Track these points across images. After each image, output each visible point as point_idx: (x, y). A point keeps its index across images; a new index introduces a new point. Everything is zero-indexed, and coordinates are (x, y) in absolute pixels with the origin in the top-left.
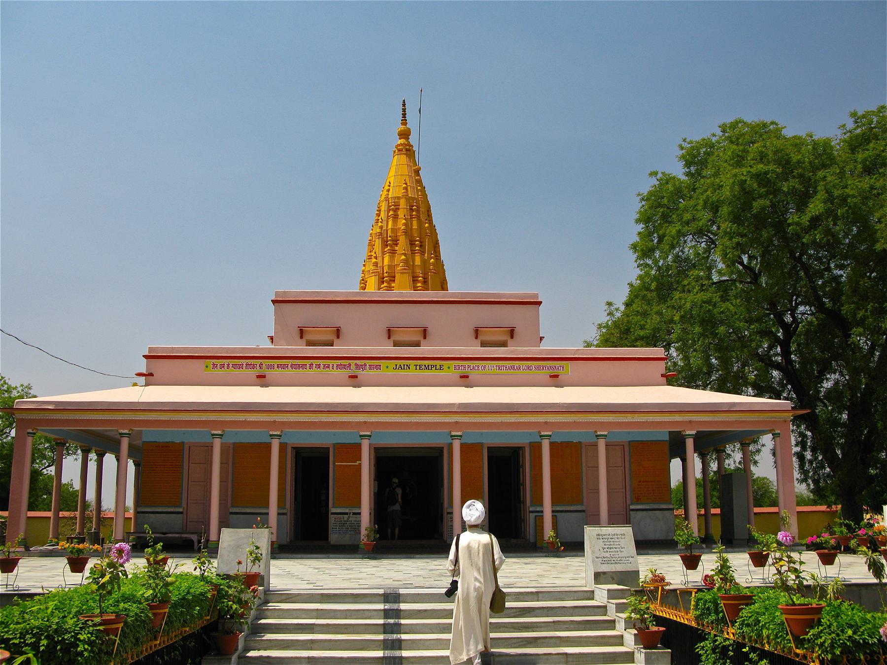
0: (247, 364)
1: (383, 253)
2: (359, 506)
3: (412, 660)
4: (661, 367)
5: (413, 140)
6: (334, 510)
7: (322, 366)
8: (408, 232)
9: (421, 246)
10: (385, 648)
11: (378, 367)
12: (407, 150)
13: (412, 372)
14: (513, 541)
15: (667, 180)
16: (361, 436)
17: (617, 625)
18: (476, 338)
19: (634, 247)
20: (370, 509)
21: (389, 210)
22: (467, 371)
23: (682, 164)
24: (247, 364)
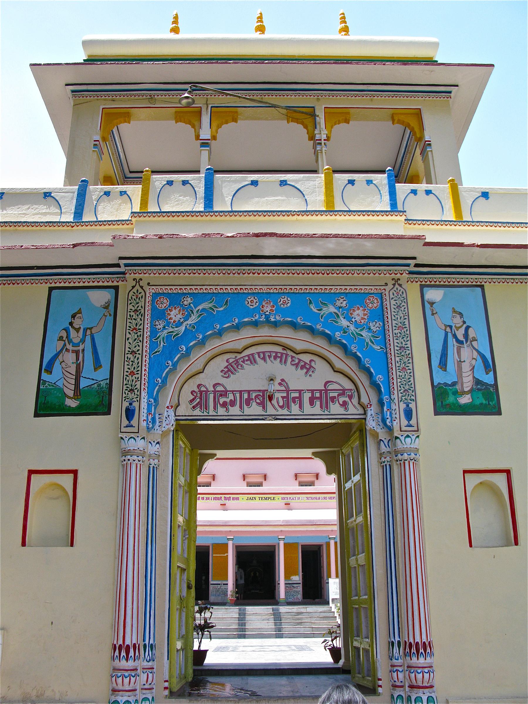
0: (225, 497)
2: (227, 579)
6: (212, 582)
7: (205, 499)
11: (238, 499)
13: (257, 502)
16: (228, 539)
18: (244, 480)
20: (233, 581)
22: (289, 501)
24: (225, 497)
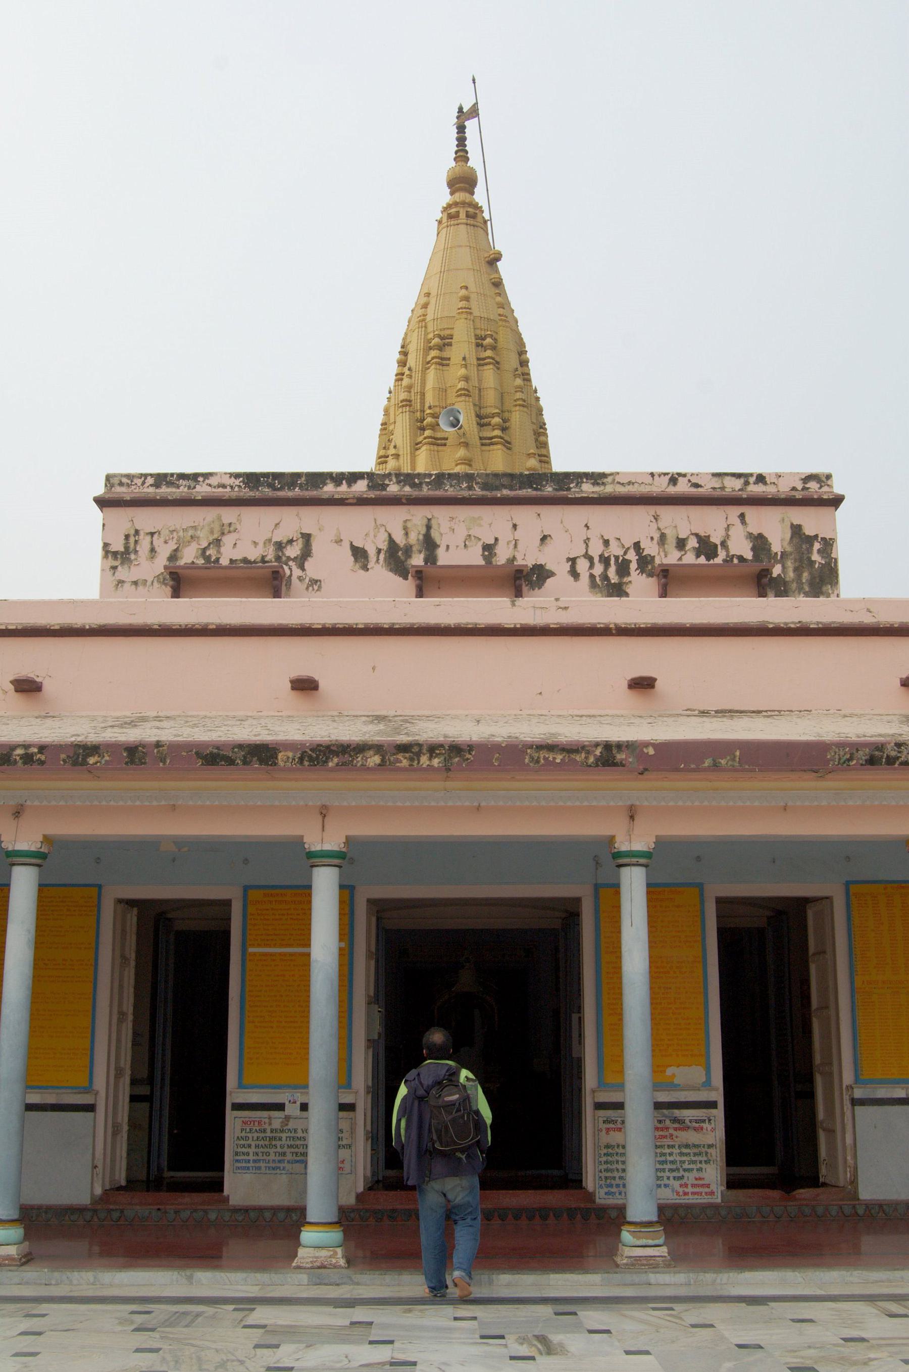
1: (416, 446)
5: (479, 196)
9: (504, 429)
12: (468, 216)
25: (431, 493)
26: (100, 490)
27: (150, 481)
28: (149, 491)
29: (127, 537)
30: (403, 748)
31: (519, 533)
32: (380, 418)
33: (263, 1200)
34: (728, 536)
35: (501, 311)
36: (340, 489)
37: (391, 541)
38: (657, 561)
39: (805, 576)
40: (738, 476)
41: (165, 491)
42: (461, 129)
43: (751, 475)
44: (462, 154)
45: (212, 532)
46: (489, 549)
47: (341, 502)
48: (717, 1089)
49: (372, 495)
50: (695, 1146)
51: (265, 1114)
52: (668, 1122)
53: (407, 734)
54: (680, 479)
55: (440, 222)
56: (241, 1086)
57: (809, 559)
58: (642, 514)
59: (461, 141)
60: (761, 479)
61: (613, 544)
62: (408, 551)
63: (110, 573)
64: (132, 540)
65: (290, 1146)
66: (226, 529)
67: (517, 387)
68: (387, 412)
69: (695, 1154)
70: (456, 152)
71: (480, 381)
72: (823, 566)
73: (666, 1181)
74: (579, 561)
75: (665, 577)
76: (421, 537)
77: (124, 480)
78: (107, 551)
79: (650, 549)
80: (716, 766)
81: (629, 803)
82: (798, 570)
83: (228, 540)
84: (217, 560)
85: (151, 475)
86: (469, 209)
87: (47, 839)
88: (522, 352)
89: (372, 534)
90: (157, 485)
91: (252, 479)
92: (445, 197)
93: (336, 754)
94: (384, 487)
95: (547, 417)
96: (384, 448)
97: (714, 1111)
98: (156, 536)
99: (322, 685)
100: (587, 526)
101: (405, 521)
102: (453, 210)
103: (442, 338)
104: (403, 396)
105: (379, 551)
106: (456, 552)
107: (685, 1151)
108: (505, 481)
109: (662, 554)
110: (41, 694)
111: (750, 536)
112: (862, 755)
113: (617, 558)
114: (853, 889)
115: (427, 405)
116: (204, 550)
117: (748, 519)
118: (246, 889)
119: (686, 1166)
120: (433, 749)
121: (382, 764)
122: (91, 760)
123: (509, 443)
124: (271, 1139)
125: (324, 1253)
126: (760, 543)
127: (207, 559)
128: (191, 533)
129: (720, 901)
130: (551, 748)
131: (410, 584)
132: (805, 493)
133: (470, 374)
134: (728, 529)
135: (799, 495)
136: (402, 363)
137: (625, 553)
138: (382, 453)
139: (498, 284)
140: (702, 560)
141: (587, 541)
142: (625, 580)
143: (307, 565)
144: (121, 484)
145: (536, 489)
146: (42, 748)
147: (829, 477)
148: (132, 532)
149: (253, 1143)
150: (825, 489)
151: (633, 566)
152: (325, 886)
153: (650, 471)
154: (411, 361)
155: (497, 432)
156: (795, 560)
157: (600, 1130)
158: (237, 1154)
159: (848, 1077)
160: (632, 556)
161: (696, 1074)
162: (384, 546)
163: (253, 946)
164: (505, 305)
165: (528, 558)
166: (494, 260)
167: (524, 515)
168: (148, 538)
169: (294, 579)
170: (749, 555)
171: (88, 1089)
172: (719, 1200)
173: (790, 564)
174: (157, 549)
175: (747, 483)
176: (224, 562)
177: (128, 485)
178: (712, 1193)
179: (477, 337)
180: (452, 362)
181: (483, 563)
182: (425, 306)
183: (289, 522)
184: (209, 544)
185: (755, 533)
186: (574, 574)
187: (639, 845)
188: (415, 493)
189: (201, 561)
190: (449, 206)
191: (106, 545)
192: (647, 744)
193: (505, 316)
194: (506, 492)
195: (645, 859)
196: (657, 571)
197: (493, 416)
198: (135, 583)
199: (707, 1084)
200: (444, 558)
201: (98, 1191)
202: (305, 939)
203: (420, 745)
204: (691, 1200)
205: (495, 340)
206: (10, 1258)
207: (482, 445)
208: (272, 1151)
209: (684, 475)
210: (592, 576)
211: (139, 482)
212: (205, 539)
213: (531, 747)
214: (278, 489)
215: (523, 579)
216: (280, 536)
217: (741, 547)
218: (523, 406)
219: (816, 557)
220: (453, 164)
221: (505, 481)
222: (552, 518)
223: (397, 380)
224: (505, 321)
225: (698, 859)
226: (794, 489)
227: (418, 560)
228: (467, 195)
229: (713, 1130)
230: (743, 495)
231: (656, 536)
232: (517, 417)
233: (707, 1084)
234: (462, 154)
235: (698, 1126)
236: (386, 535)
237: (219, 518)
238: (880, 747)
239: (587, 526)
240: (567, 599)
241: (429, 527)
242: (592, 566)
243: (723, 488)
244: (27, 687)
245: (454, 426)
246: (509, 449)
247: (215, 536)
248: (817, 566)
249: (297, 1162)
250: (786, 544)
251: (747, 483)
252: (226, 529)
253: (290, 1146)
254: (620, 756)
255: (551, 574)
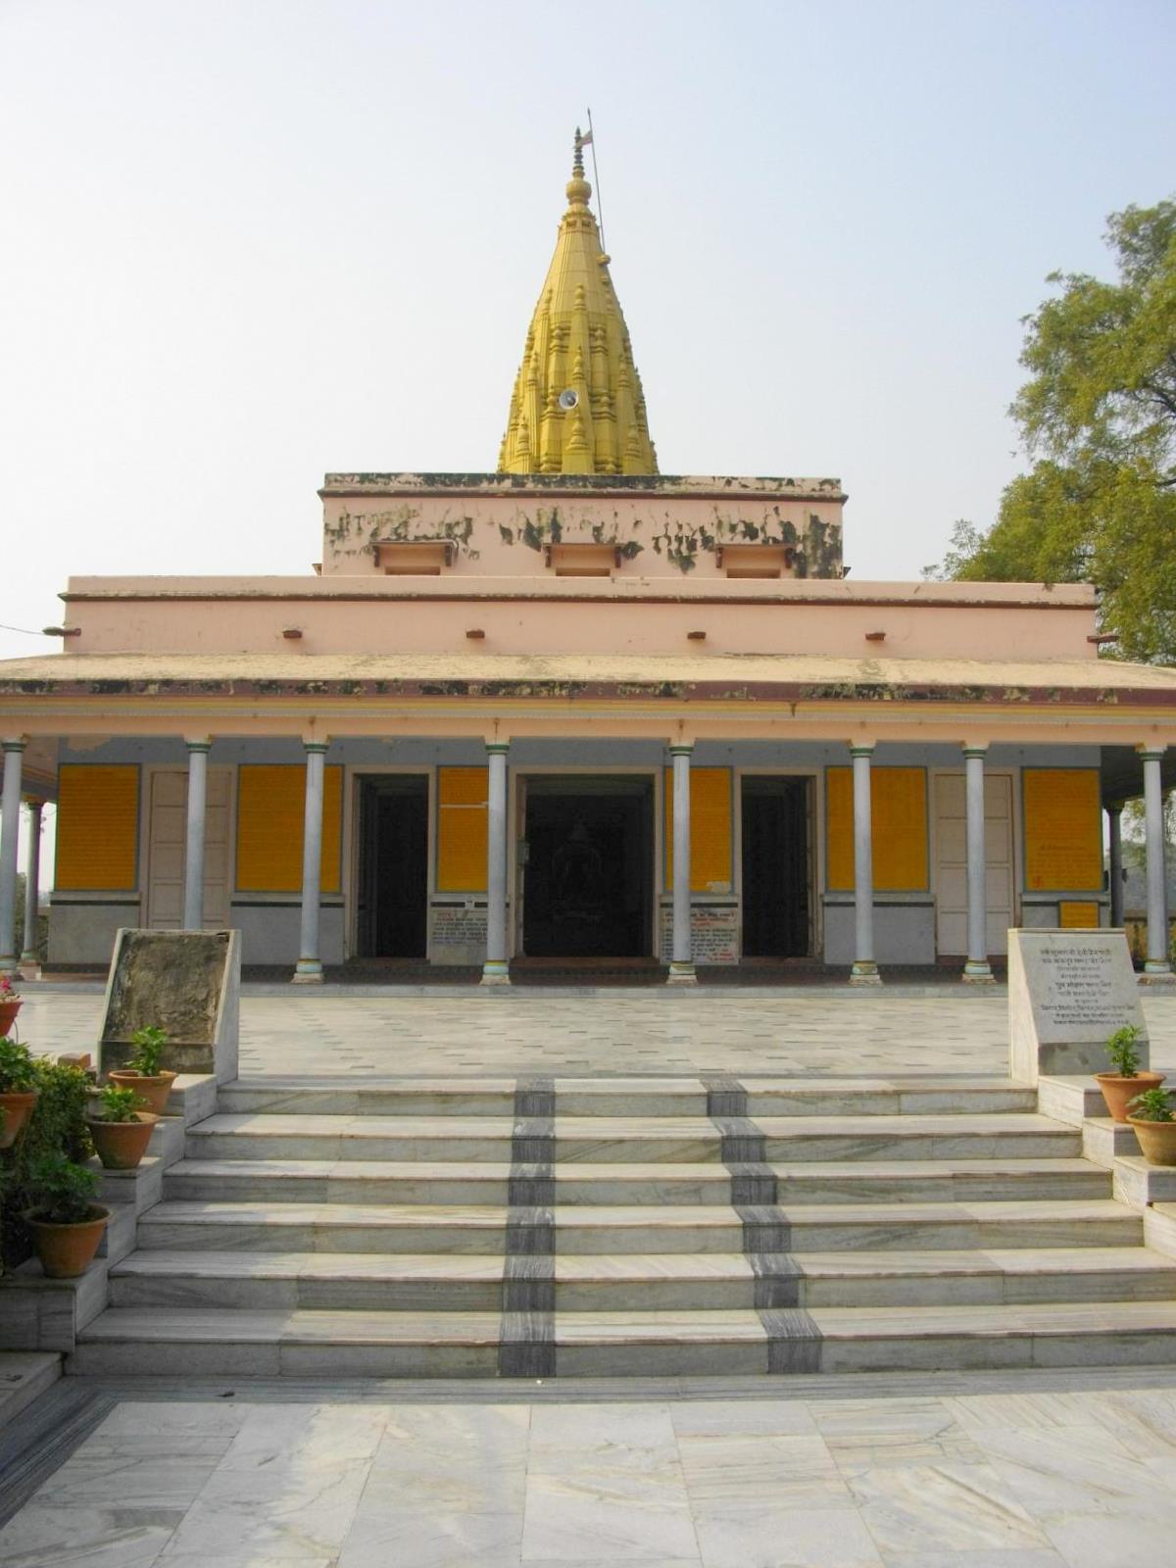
1: (540, 419)
3: (582, 1289)
4: (1092, 623)
5: (593, 206)
8: (586, 376)
9: (610, 405)
10: (512, 1249)
12: (584, 224)
14: (791, 961)
15: (1082, 287)
17: (1118, 1187)
19: (1013, 410)
21: (550, 338)
23: (1115, 252)
25: (557, 489)
26: (321, 485)
27: (357, 478)
28: (357, 486)
29: (341, 519)
30: (544, 684)
31: (622, 519)
32: (511, 391)
33: (452, 962)
34: (766, 523)
35: (609, 306)
36: (492, 486)
37: (529, 524)
38: (716, 541)
39: (819, 553)
40: (774, 480)
41: (367, 487)
42: (579, 150)
43: (784, 479)
44: (579, 171)
45: (401, 516)
46: (597, 530)
47: (493, 495)
48: (738, 896)
49: (516, 490)
50: (724, 930)
51: (452, 909)
52: (706, 916)
53: (546, 673)
54: (734, 482)
55: (561, 229)
56: (437, 891)
57: (822, 540)
58: (706, 506)
59: (579, 158)
60: (790, 482)
61: (685, 527)
62: (540, 531)
63: (329, 545)
64: (345, 521)
65: (469, 929)
66: (412, 514)
67: (623, 370)
68: (517, 385)
69: (723, 935)
70: (575, 168)
71: (592, 366)
72: (831, 546)
73: (704, 952)
74: (661, 539)
75: (720, 553)
76: (550, 521)
77: (339, 478)
78: (328, 530)
79: (711, 531)
80: (732, 697)
81: (680, 718)
82: (814, 548)
83: (413, 522)
84: (405, 536)
85: (358, 474)
86: (584, 219)
87: (330, 738)
88: (626, 340)
89: (515, 518)
90: (362, 482)
91: (430, 478)
92: (565, 207)
93: (504, 687)
94: (523, 485)
95: (645, 391)
96: (516, 418)
97: (736, 909)
98: (362, 519)
99: (486, 634)
100: (667, 515)
101: (539, 510)
102: (570, 220)
103: (562, 329)
104: (530, 376)
105: (520, 531)
106: (575, 533)
107: (716, 933)
108: (609, 481)
109: (719, 535)
110: (301, 639)
111: (781, 523)
112: (820, 691)
113: (687, 537)
114: (830, 771)
115: (550, 385)
116: (396, 529)
117: (780, 511)
118: (438, 767)
119: (717, 942)
120: (562, 684)
121: (532, 694)
122: (355, 690)
123: (615, 417)
124: (456, 924)
125: (497, 977)
126: (788, 528)
127: (399, 536)
128: (386, 517)
129: (744, 778)
130: (633, 684)
131: (540, 557)
132: (822, 493)
133: (589, 363)
134: (766, 517)
135: (816, 494)
136: (530, 347)
137: (693, 534)
138: (513, 421)
139: (608, 283)
140: (747, 541)
141: (667, 525)
142: (693, 553)
143: (469, 540)
144: (336, 481)
145: (631, 487)
146: (326, 682)
147: (838, 481)
148: (345, 516)
149: (445, 927)
150: (836, 490)
151: (699, 543)
152: (497, 765)
153: (712, 475)
154: (538, 346)
155: (605, 409)
156: (813, 541)
157: (663, 920)
158: (435, 933)
159: (821, 889)
160: (698, 537)
161: (726, 886)
162: (523, 527)
163: (444, 803)
164: (614, 301)
165: (623, 539)
166: (604, 264)
167: (622, 505)
168: (356, 520)
169: (460, 550)
170: (780, 537)
171: (340, 894)
172: (737, 963)
173: (809, 544)
174: (363, 528)
175: (780, 485)
176: (411, 537)
177: (341, 482)
178: (733, 959)
179: (590, 329)
180: (569, 350)
181: (593, 541)
182: (549, 301)
183: (456, 510)
184: (400, 525)
185: (785, 521)
186: (657, 549)
187: (686, 743)
188: (546, 490)
189: (394, 537)
190: (569, 215)
191: (326, 525)
192: (691, 683)
193: (613, 308)
194: (610, 490)
195: (689, 751)
196: (715, 547)
197: (602, 395)
198: (348, 553)
199: (732, 892)
200: (566, 537)
201: (347, 956)
202: (484, 796)
203: (554, 682)
204: (719, 963)
205: (605, 331)
206: (316, 980)
207: (594, 418)
208: (457, 932)
209: (736, 479)
210: (670, 551)
211: (348, 479)
212: (395, 526)
213: (621, 683)
214: (449, 486)
215: (624, 553)
216: (449, 520)
217: (775, 531)
218: (626, 386)
219: (827, 539)
220: (572, 179)
221: (609, 481)
222: (643, 509)
223: (526, 362)
224: (613, 315)
225: (730, 750)
226: (814, 490)
227: (547, 539)
228: (583, 206)
229: (735, 920)
230: (776, 493)
231: (716, 522)
232: (622, 396)
233: (732, 892)
234: (579, 171)
235: (725, 918)
236: (525, 520)
237: (406, 506)
238: (831, 686)
239: (667, 515)
240: (655, 573)
241: (555, 514)
242: (670, 544)
243: (763, 489)
244: (293, 635)
245: (571, 404)
246: (615, 421)
247: (403, 519)
248: (827, 545)
249: (473, 938)
250: (806, 529)
251: (780, 485)
252: (411, 514)
253: (469, 929)
254: (675, 690)
255: (641, 549)
